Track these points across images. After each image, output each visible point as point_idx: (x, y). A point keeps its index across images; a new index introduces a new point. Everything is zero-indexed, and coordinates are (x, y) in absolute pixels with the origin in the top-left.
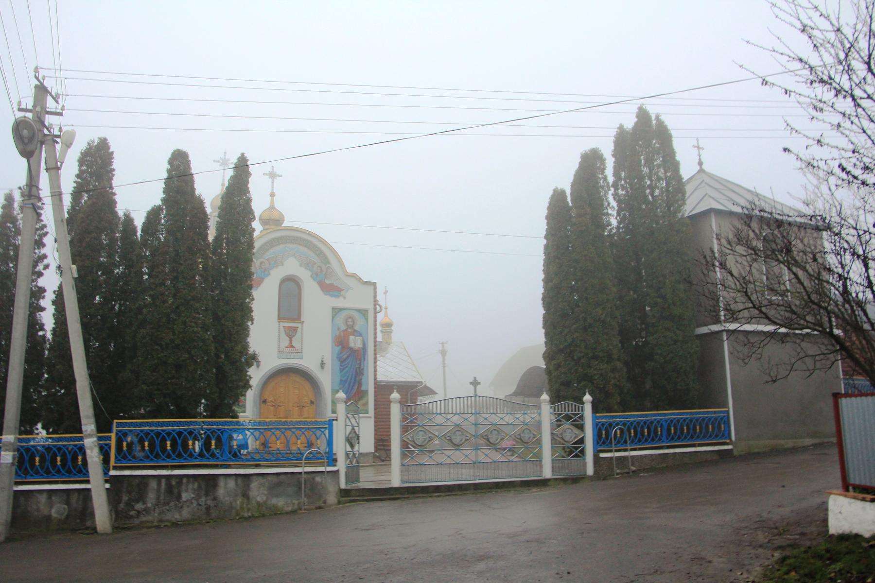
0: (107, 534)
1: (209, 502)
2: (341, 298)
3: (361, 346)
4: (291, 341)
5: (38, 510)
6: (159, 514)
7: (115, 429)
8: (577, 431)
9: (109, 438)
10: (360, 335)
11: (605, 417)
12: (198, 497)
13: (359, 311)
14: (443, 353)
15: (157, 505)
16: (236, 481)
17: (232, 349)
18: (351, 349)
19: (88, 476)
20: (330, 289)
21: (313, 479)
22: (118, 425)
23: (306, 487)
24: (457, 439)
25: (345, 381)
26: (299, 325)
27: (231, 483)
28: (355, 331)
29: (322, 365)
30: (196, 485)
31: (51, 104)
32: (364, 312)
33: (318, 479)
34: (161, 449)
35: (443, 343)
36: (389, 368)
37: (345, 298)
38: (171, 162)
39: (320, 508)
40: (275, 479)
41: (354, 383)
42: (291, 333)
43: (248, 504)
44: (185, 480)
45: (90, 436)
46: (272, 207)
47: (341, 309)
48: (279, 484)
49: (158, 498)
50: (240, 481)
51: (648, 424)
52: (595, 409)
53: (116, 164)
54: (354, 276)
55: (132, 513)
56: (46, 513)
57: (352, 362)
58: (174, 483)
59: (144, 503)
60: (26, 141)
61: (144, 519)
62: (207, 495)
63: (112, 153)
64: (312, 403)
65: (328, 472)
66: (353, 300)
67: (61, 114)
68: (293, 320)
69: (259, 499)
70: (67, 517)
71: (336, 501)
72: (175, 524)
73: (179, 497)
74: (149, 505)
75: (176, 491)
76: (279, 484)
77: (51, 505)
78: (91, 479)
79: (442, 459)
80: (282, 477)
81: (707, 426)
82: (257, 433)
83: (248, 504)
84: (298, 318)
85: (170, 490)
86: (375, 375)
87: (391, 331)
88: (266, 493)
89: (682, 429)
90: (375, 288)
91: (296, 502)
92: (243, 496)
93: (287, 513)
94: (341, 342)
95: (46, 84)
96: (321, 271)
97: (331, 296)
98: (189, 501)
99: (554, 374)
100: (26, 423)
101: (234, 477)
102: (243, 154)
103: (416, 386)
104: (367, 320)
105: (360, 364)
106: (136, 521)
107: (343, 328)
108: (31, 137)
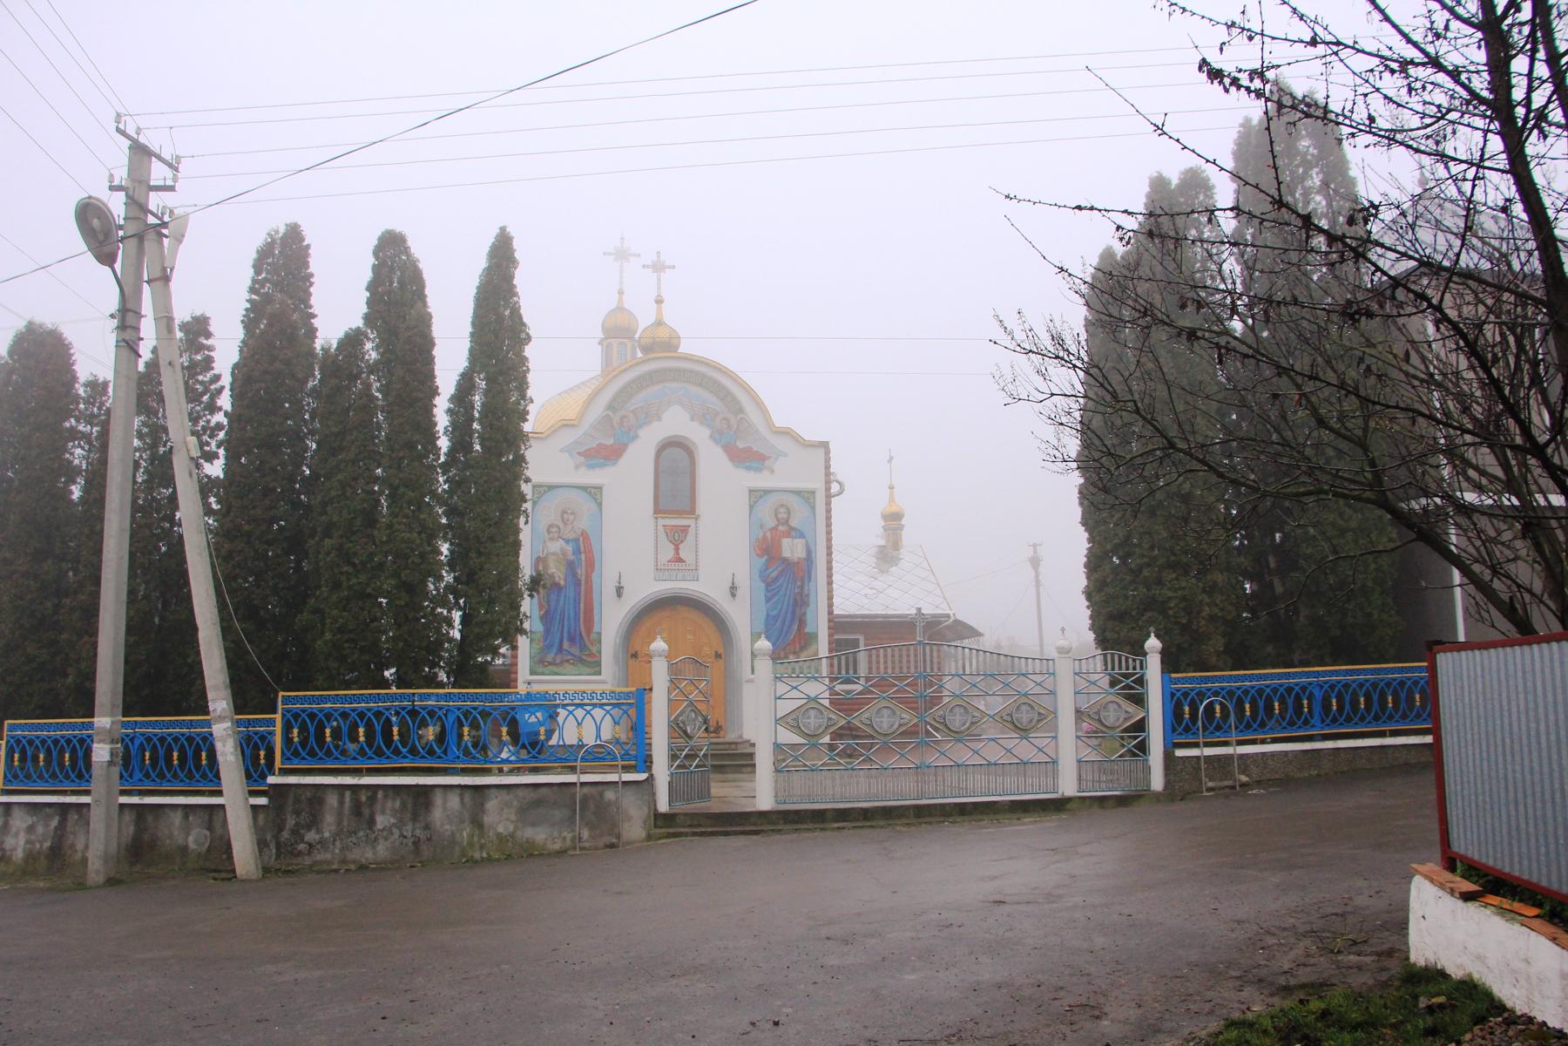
0: (250, 881)
1: (418, 832)
2: (766, 473)
3: (804, 555)
4: (677, 549)
5: (171, 836)
6: (342, 849)
7: (280, 706)
8: (1130, 707)
9: (272, 722)
10: (802, 536)
11: (1189, 680)
12: (401, 823)
13: (798, 493)
14: (1035, 562)
15: (337, 835)
16: (461, 796)
17: (481, 569)
18: (785, 560)
19: (219, 784)
20: (746, 457)
21: (601, 795)
22: (286, 700)
23: (591, 808)
24: (1024, 717)
25: (776, 618)
26: (691, 522)
27: (454, 801)
28: (792, 529)
29: (733, 590)
30: (398, 804)
31: (158, 173)
32: (807, 496)
33: (610, 795)
34: (312, 742)
35: (1035, 546)
36: (856, 588)
37: (772, 471)
38: (377, 252)
39: (612, 846)
40: (531, 795)
41: (793, 620)
42: (677, 536)
43: (482, 835)
44: (380, 794)
45: (221, 719)
46: (659, 323)
47: (767, 492)
48: (538, 803)
49: (339, 823)
50: (467, 797)
51: (1342, 690)
52: (1171, 662)
53: (315, 265)
54: (787, 433)
55: (301, 847)
56: (181, 841)
57: (787, 581)
58: (364, 799)
59: (319, 831)
60: (101, 237)
61: (319, 857)
62: (415, 819)
63: (308, 247)
64: (718, 656)
65: (625, 783)
66: (789, 474)
67: (171, 189)
68: (679, 513)
69: (501, 829)
70: (209, 850)
71: (643, 834)
72: (363, 868)
73: (371, 822)
74: (327, 835)
75: (366, 811)
76: (538, 803)
77: (187, 830)
78: (225, 789)
79: (994, 754)
80: (544, 790)
81: (1383, 697)
82: (616, 712)
83: (482, 835)
84: (691, 511)
85: (357, 810)
86: (830, 605)
87: (901, 528)
88: (513, 818)
89: (1410, 698)
90: (827, 452)
91: (569, 836)
92: (473, 822)
93: (550, 854)
94: (767, 549)
95: (142, 139)
96: (729, 427)
97: (748, 469)
98: (389, 830)
99: (1097, 598)
100: (385, 684)
101: (458, 791)
102: (503, 229)
103: (940, 623)
104: (813, 508)
105: (802, 587)
106: (308, 861)
107: (771, 523)
108: (124, 235)
